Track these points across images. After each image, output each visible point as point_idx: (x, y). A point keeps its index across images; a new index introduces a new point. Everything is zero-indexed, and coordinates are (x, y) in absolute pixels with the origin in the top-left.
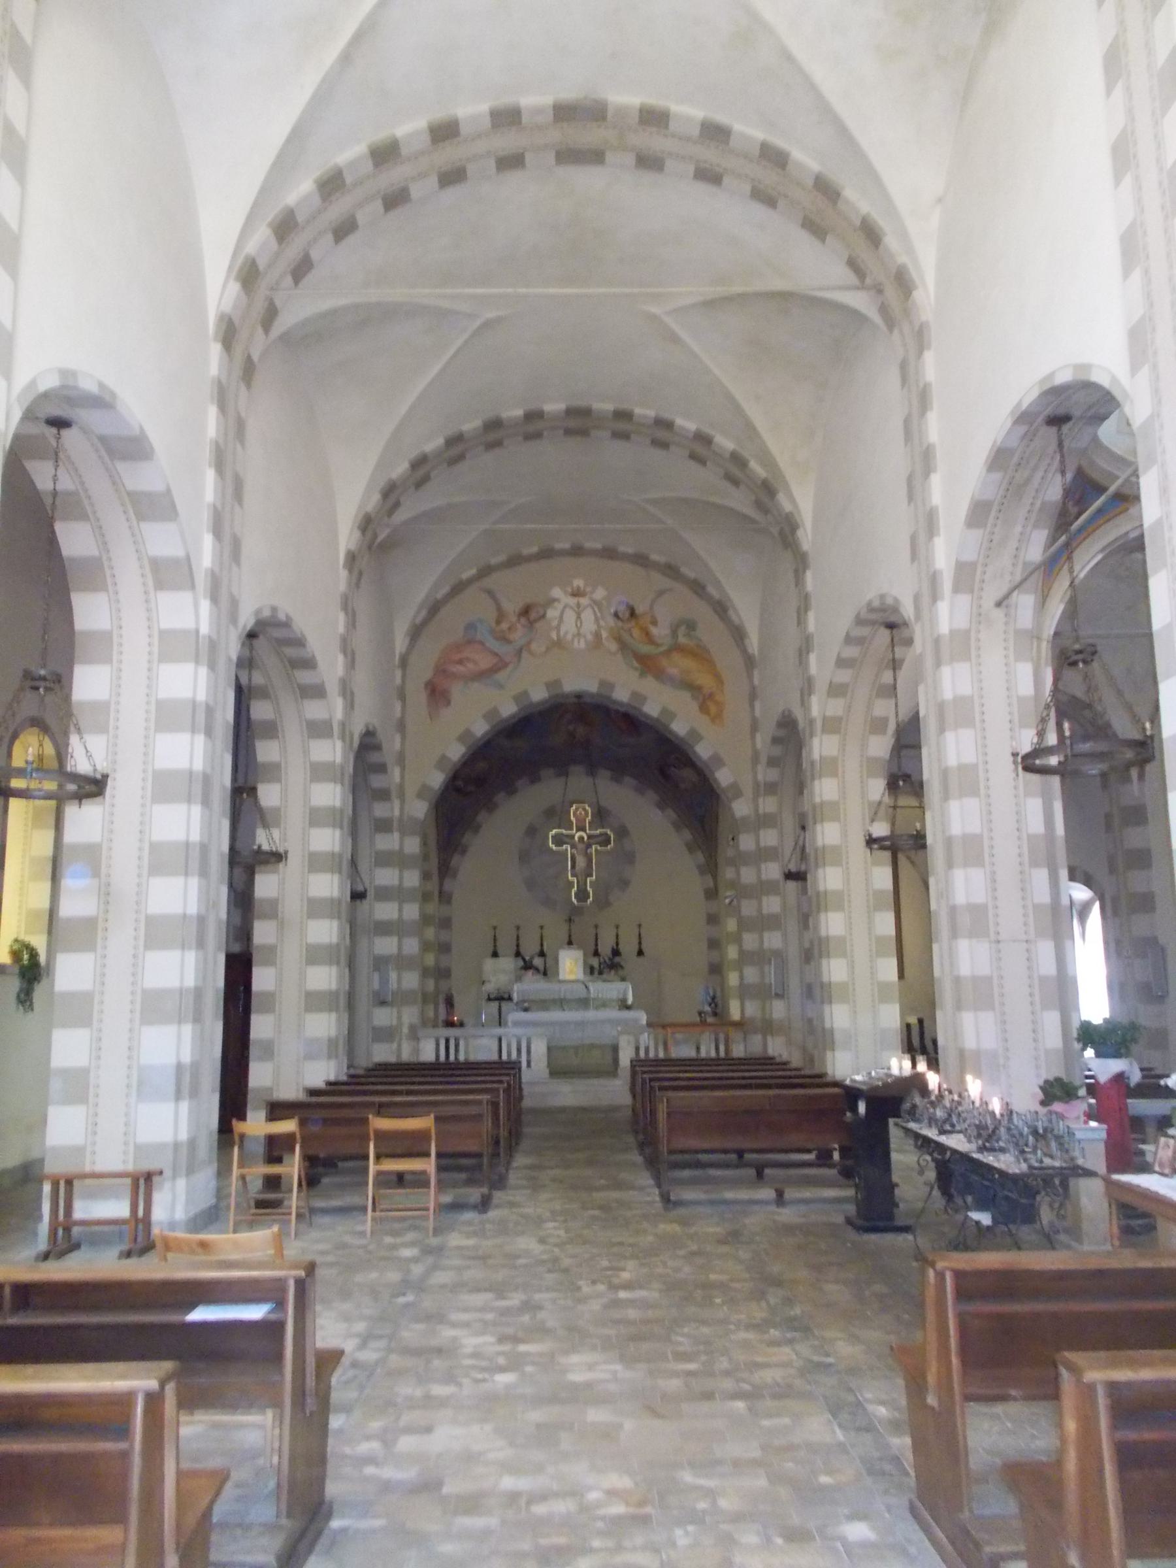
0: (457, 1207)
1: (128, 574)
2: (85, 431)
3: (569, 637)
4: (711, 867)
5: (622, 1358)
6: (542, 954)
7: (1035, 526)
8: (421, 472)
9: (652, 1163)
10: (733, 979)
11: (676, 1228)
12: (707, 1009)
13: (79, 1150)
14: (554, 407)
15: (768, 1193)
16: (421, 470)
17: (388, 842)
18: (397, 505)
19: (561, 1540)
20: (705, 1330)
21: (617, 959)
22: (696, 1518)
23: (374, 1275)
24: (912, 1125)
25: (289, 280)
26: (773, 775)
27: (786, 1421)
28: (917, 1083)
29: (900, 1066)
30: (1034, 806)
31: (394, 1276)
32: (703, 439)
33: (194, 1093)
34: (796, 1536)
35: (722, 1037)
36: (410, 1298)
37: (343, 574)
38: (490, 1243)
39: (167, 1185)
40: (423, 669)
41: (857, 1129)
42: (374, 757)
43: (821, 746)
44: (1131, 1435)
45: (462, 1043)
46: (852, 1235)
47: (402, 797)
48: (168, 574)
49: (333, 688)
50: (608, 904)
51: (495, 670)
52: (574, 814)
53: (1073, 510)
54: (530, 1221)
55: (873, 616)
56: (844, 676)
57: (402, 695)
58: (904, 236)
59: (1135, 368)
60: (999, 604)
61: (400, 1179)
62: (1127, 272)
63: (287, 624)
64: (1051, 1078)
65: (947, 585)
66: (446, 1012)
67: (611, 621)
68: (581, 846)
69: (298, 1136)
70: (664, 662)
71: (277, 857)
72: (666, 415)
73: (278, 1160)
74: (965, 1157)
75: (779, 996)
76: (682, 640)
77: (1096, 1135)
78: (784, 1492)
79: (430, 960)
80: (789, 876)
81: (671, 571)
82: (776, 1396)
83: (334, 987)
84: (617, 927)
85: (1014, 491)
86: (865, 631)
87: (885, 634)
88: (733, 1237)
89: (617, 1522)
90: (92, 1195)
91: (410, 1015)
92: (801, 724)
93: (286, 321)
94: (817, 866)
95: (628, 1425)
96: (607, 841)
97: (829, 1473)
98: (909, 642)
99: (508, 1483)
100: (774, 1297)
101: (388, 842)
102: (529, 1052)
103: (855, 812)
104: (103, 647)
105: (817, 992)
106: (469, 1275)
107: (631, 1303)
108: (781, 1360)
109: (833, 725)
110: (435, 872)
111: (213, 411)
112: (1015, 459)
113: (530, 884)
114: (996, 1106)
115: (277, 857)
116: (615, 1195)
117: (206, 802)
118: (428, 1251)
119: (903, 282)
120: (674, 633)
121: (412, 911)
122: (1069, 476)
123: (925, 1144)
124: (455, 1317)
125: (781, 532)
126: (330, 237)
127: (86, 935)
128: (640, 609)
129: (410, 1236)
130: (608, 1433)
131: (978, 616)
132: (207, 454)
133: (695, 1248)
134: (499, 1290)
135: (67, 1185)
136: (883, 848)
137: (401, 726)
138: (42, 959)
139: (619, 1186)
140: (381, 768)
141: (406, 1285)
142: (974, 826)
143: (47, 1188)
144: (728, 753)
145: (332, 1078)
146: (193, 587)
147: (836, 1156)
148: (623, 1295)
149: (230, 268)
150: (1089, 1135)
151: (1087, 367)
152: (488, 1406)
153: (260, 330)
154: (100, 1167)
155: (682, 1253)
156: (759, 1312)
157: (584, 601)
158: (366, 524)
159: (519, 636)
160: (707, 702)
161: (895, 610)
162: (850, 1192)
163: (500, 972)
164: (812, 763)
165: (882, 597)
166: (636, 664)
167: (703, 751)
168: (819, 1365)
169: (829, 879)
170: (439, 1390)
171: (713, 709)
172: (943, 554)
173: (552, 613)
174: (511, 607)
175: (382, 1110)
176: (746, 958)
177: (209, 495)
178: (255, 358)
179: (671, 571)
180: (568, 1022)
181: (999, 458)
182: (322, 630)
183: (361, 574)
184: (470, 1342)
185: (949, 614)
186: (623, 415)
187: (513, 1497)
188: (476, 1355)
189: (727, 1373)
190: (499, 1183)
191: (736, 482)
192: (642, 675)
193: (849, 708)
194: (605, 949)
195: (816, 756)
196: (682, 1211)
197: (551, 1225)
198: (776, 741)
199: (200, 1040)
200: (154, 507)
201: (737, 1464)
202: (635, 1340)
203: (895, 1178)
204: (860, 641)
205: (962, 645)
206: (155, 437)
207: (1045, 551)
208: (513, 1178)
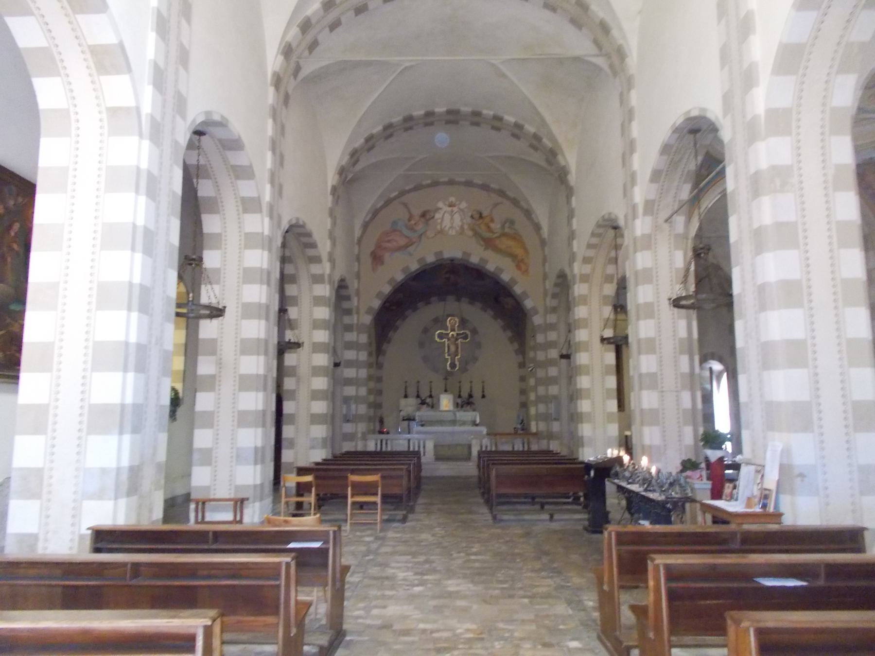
0: (388, 521)
1: (230, 206)
2: (212, 137)
3: (447, 228)
4: (522, 350)
5: (472, 582)
6: (431, 396)
7: (685, 182)
8: (370, 144)
9: (488, 502)
10: (532, 411)
11: (499, 531)
12: (519, 426)
13: (208, 488)
14: (440, 109)
15: (546, 516)
16: (370, 143)
17: (351, 337)
18: (357, 161)
19: (445, 645)
20: (512, 572)
21: (471, 400)
22: (505, 639)
23: (353, 548)
24: (616, 481)
25: (306, 53)
26: (554, 303)
27: (546, 606)
28: (619, 460)
29: (612, 453)
30: (682, 324)
31: (363, 548)
32: (518, 126)
33: (263, 462)
34: (546, 645)
35: (526, 440)
36: (371, 557)
37: (330, 198)
38: (408, 536)
39: (251, 505)
40: (369, 246)
41: (589, 484)
42: (344, 292)
43: (579, 289)
44: (674, 585)
45: (389, 442)
46: (587, 535)
47: (358, 313)
48: (250, 205)
49: (325, 257)
50: (466, 370)
51: (407, 246)
52: (449, 322)
53: (704, 172)
54: (427, 527)
55: (607, 223)
56: (591, 253)
57: (358, 259)
58: (621, 29)
59: (726, 112)
60: (666, 221)
61: (361, 506)
62: (722, 68)
63: (303, 226)
64: (686, 459)
65: (640, 210)
66: (380, 427)
67: (469, 220)
68: (453, 340)
69: (314, 483)
70: (497, 242)
71: (298, 345)
72: (500, 114)
73: (302, 495)
74: (637, 494)
75: (556, 419)
76: (507, 230)
77: (705, 486)
78: (543, 631)
79: (372, 398)
80: (563, 356)
81: (501, 193)
82: (542, 598)
83: (325, 412)
84: (471, 382)
85: (673, 165)
86: (601, 230)
87: (611, 233)
88: (527, 534)
89: (469, 640)
90: (216, 510)
91: (361, 427)
92: (569, 277)
93: (305, 72)
94: (576, 352)
95: (475, 607)
96: (466, 337)
97: (564, 624)
98: (622, 236)
99: (422, 626)
100: (545, 559)
101: (351, 337)
102: (424, 447)
103: (596, 324)
104: (217, 241)
105: (576, 418)
106: (398, 548)
107: (477, 561)
108: (546, 584)
109: (585, 278)
110: (374, 353)
111: (270, 122)
112: (674, 149)
113: (425, 359)
114: (653, 470)
115: (298, 345)
116: (470, 516)
117: (267, 319)
118: (377, 538)
119: (621, 53)
120: (503, 227)
121: (363, 373)
122: (700, 158)
123: (620, 488)
124: (393, 565)
125: (559, 176)
126: (327, 29)
127: (211, 383)
128: (485, 214)
129: (369, 532)
130: (465, 610)
131: (656, 227)
132: (268, 144)
133: (508, 539)
134: (414, 555)
135: (202, 504)
136: (609, 343)
137: (358, 276)
138: (181, 395)
139: (470, 512)
140: (348, 298)
141: (368, 552)
142: (652, 334)
143: (193, 506)
144: (531, 291)
145: (324, 457)
146: (261, 211)
147: (582, 499)
148: (473, 557)
149: (279, 49)
150: (701, 485)
151: (704, 110)
152: (411, 598)
153: (292, 77)
154: (217, 496)
155: (501, 541)
156: (538, 565)
157: (455, 209)
158: (342, 171)
159: (420, 227)
160: (520, 264)
161: (616, 220)
162: (586, 516)
163: (409, 405)
164: (574, 298)
165: (610, 214)
166: (482, 243)
167: (518, 290)
168: (563, 587)
169: (582, 358)
170: (388, 593)
171: (523, 267)
172: (640, 194)
173: (438, 216)
174: (417, 212)
175: (353, 472)
176: (540, 399)
177: (269, 164)
178: (290, 92)
179: (501, 193)
180: (444, 432)
181: (666, 149)
182: (320, 228)
183: (338, 197)
184: (401, 575)
185: (641, 226)
186: (477, 114)
187: (424, 631)
188: (404, 580)
189: (521, 588)
190: (411, 510)
191: (536, 149)
192: (486, 249)
193: (593, 269)
194: (465, 394)
195: (576, 294)
196: (502, 524)
197: (437, 529)
198: (556, 285)
199: (265, 435)
200: (244, 173)
201: (523, 622)
202: (477, 575)
203: (608, 509)
204: (599, 235)
205: (648, 242)
206: (245, 140)
207: (691, 192)
208: (418, 508)
